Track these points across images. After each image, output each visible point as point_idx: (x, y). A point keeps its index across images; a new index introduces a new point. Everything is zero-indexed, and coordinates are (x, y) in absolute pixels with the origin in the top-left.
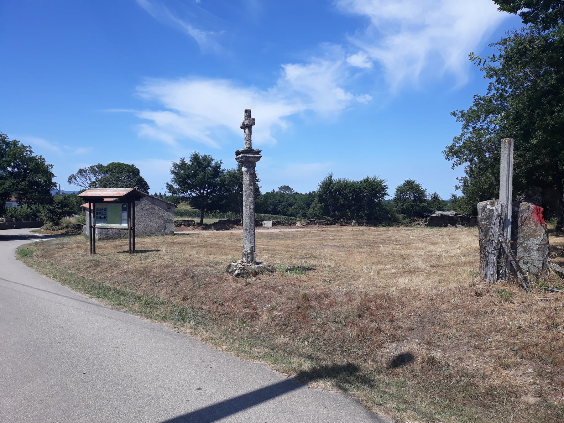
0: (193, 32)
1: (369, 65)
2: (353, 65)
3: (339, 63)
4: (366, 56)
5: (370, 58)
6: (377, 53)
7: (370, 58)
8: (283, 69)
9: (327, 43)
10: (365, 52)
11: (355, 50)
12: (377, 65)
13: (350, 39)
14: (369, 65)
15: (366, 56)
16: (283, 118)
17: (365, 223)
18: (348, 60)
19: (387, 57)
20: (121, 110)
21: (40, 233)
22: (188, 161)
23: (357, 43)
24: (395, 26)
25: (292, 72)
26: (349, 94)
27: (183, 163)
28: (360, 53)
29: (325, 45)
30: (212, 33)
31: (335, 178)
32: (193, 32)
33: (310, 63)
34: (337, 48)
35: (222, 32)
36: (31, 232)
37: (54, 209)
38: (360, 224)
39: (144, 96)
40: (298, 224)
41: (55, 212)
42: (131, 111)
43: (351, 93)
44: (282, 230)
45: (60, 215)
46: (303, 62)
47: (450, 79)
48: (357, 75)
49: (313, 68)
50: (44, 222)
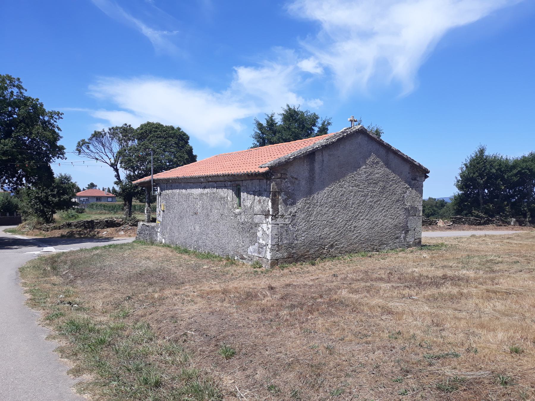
0: (147, 31)
1: (319, 71)
2: (305, 70)
3: (291, 68)
4: (317, 62)
5: (320, 64)
6: (326, 59)
7: (320, 64)
8: (236, 72)
9: (280, 48)
10: (317, 58)
11: (308, 55)
12: (328, 71)
13: (302, 43)
14: (319, 71)
15: (317, 62)
16: (237, 121)
17: (530, 222)
18: (299, 65)
19: (338, 64)
20: (76, 109)
21: (23, 234)
22: (279, 120)
23: (309, 48)
24: (345, 32)
25: (245, 75)
26: (301, 98)
27: (271, 123)
28: (312, 59)
29: (278, 49)
30: (165, 32)
31: (489, 153)
32: (147, 31)
33: (263, 67)
34: (290, 53)
35: (175, 32)
36: (5, 231)
37: (47, 197)
38: (521, 223)
39: (98, 95)
40: (440, 223)
41: (48, 202)
42: (86, 110)
43: (303, 98)
44: (517, 232)
45: (53, 207)
46: (255, 65)
47: (396, 86)
48: (309, 81)
49: (266, 72)
50: (23, 218)
